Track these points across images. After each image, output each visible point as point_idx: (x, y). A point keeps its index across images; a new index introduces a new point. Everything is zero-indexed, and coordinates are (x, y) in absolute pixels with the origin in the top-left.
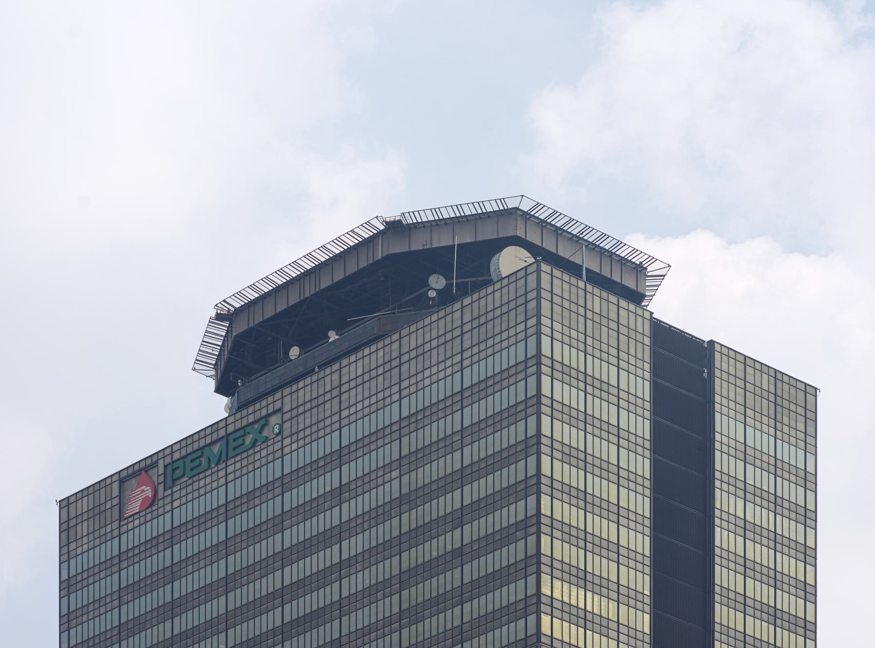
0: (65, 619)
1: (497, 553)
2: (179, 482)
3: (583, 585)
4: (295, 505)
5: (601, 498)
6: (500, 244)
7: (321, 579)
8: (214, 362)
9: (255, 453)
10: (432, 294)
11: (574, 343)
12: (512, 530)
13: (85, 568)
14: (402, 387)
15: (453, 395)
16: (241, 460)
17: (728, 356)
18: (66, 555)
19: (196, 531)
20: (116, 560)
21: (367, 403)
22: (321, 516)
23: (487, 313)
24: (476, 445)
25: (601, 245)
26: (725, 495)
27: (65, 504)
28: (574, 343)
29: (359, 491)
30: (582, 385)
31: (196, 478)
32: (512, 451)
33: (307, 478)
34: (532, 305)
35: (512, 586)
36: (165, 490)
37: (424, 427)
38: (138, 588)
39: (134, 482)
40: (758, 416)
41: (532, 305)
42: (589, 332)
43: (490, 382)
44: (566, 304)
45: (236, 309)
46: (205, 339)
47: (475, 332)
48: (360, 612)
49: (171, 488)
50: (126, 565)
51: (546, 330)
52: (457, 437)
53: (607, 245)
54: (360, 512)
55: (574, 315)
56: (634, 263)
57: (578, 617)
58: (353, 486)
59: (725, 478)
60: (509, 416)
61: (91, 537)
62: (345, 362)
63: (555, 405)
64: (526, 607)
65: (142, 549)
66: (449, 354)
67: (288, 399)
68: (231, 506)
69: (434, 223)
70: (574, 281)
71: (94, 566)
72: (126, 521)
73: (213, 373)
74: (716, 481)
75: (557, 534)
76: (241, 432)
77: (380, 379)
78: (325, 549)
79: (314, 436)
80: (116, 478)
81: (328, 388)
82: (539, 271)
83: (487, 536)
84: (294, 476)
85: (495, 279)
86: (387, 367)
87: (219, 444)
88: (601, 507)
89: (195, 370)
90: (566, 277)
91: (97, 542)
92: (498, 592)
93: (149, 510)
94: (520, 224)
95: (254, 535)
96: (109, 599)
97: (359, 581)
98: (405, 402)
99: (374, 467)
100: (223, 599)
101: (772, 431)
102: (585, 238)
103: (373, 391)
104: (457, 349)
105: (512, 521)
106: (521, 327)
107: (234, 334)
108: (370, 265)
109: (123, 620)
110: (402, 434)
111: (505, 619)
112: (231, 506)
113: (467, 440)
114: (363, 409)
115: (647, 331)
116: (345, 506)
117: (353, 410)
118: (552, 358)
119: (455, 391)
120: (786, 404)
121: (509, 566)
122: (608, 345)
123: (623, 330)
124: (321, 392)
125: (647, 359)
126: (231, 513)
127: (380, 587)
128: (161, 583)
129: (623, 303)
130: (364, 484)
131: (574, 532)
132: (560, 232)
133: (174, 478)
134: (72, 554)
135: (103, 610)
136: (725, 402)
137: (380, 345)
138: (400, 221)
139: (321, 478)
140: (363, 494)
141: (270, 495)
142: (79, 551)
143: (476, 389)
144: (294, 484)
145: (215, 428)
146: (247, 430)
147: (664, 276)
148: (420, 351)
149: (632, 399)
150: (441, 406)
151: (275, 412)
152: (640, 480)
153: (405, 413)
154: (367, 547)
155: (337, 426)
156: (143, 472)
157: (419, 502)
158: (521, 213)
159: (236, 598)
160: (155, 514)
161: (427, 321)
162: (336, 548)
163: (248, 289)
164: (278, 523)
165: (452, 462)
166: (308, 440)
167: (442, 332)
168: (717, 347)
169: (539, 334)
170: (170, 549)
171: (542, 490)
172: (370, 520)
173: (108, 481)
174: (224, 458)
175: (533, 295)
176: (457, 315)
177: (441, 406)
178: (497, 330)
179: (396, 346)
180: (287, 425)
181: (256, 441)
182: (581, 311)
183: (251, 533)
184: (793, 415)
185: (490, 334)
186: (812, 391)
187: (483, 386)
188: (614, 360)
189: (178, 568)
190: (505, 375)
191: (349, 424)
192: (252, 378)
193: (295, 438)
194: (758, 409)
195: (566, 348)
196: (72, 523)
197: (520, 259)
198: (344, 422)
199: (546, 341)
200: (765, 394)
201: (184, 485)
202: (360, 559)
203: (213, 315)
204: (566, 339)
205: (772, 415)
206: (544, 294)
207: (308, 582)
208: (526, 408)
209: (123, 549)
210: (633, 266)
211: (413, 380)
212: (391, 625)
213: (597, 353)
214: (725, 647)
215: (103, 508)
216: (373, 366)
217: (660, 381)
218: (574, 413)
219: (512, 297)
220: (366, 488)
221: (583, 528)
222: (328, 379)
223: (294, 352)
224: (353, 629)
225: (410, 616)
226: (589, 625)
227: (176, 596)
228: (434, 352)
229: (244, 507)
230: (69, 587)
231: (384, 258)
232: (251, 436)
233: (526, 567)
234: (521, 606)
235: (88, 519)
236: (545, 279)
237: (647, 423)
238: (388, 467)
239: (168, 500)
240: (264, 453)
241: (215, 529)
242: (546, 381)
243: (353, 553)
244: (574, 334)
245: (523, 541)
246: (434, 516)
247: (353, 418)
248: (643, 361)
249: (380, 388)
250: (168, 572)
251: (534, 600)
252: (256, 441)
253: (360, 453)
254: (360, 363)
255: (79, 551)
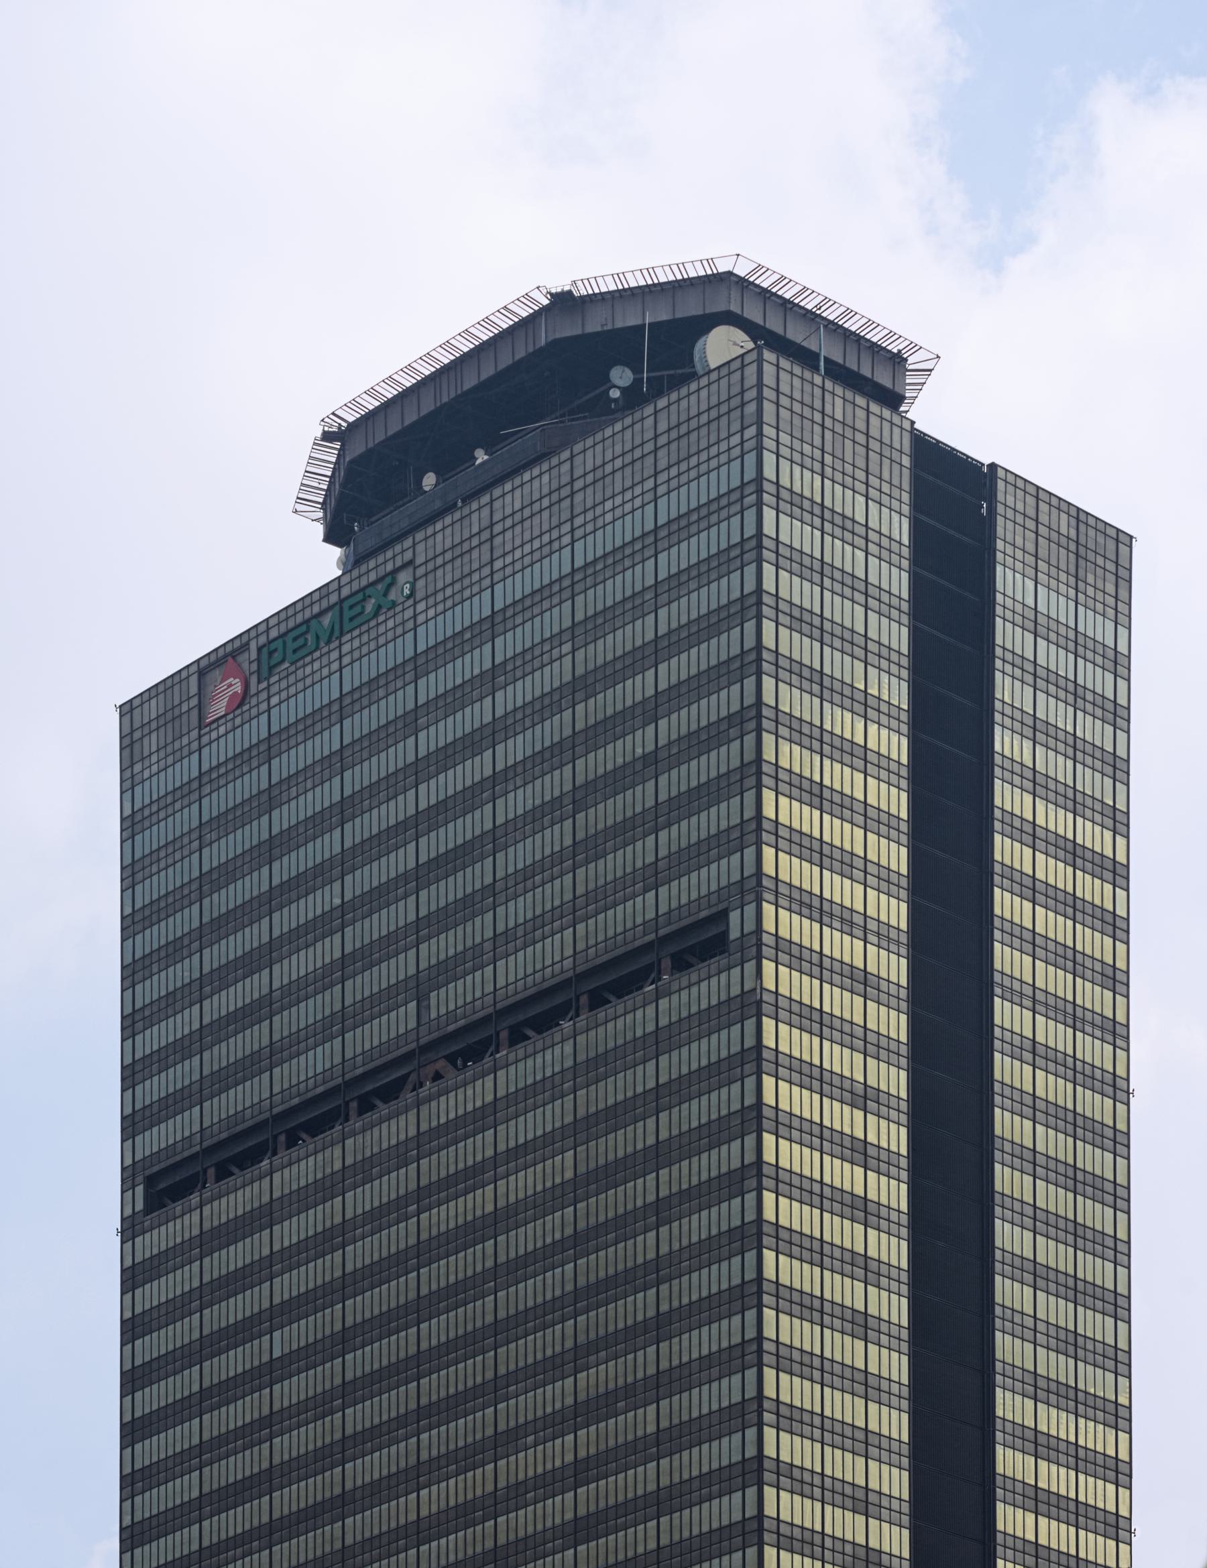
0: (128, 872)
1: (704, 758)
2: (278, 670)
3: (818, 805)
4: (432, 695)
5: (842, 682)
6: (706, 323)
7: (468, 800)
8: (321, 500)
9: (378, 625)
10: (615, 394)
11: (808, 462)
12: (724, 726)
13: (155, 797)
14: (576, 525)
15: (644, 535)
16: (360, 635)
17: (1015, 486)
18: (129, 782)
19: (300, 738)
20: (195, 785)
21: (527, 548)
22: (468, 710)
23: (689, 420)
24: (674, 605)
25: (846, 325)
26: (1008, 680)
27: (127, 710)
28: (808, 462)
29: (519, 673)
30: (817, 522)
31: (300, 663)
32: (723, 614)
33: (448, 657)
34: (751, 408)
35: (724, 805)
36: (259, 682)
37: (604, 581)
38: (224, 823)
39: (217, 674)
40: (1053, 571)
41: (751, 408)
42: (828, 448)
43: (694, 517)
44: (797, 407)
45: (349, 424)
46: (309, 469)
47: (674, 446)
48: (520, 846)
49: (268, 679)
50: (208, 791)
51: (769, 444)
52: (649, 595)
53: (853, 325)
54: (519, 703)
55: (807, 423)
56: (890, 351)
57: (811, 850)
58: (509, 667)
59: (1009, 656)
60: (719, 565)
61: (162, 754)
62: (497, 492)
63: (782, 550)
64: (742, 835)
65: (230, 766)
66: (638, 478)
67: (421, 546)
68: (347, 701)
69: (617, 295)
70: (807, 375)
71: (167, 794)
72: (207, 729)
73: (321, 515)
74: (996, 768)
75: (783, 731)
76: (360, 596)
77: (546, 514)
78: (474, 756)
79: (458, 598)
80: (194, 668)
81: (475, 530)
82: (760, 361)
83: (689, 734)
84: (431, 655)
85: (701, 372)
86: (555, 497)
87: (330, 614)
88: (842, 694)
89: (296, 512)
90: (797, 370)
91: (170, 760)
92: (704, 815)
93: (238, 712)
94: (735, 294)
95: (376, 741)
96: (186, 840)
97: (519, 801)
98: (579, 546)
99: (537, 640)
100: (337, 833)
101: (1072, 592)
102: (824, 315)
103: (536, 532)
104: (649, 471)
105: (724, 713)
106: (736, 440)
107: (347, 459)
108: (530, 354)
109: (205, 869)
110: (576, 591)
111: (714, 852)
112: (347, 701)
113: (664, 598)
114: (522, 557)
115: (907, 447)
116: (499, 695)
117: (509, 559)
118: (777, 484)
119: (647, 584)
120: (1091, 556)
121: (719, 777)
122: (854, 466)
123: (874, 445)
124: (466, 535)
125: (906, 486)
126: (347, 710)
127: (547, 809)
128: (255, 814)
129: (875, 408)
130: (526, 663)
131: (806, 729)
132: (790, 306)
133: (272, 663)
134: (138, 779)
135: (178, 856)
136: (1009, 550)
137: (545, 466)
138: (570, 292)
139: (468, 657)
140: (523, 677)
141: (399, 683)
142: (146, 774)
143: (674, 527)
144: (431, 666)
145: (324, 592)
146: (368, 592)
147: (931, 370)
148: (599, 474)
149: (885, 542)
150: (628, 551)
151: (404, 566)
152: (894, 657)
153: (579, 563)
154: (529, 753)
155: (487, 582)
156: (230, 659)
157: (599, 687)
158: (735, 279)
159: (358, 830)
160: (246, 716)
161: (608, 432)
162: (488, 754)
163: (365, 396)
164: (410, 723)
165: (643, 630)
166: (449, 603)
167: (628, 447)
168: (1001, 473)
169: (760, 449)
170: (267, 765)
171: (764, 613)
172: (534, 713)
173: (184, 675)
174: (337, 633)
175: (752, 394)
176: (649, 422)
177: (628, 551)
178: (703, 444)
179: (566, 467)
180: (421, 584)
181: (380, 607)
182: (818, 417)
183: (374, 738)
184: (1100, 571)
185: (693, 450)
186: (1127, 540)
187: (683, 523)
188: (861, 487)
189: (277, 792)
190: (714, 507)
191: (504, 579)
192: (373, 519)
193: (431, 601)
194: (1054, 562)
195: (797, 469)
196: (137, 735)
197: (735, 344)
198: (497, 577)
199: (769, 459)
200: (1063, 541)
201: (284, 674)
202: (520, 769)
203: (319, 434)
204: (797, 457)
205: (1072, 570)
206: (767, 393)
207: (450, 804)
208: (742, 553)
209: (205, 767)
210: (889, 355)
211: (590, 515)
212: (562, 863)
213: (838, 477)
214: (1010, 1566)
215: (177, 712)
216: (536, 496)
217: (923, 518)
218: (807, 561)
219: (724, 397)
220: (528, 668)
221: (818, 724)
222: (475, 516)
223: (429, 480)
224: (511, 870)
225: (587, 851)
226: (826, 861)
227: (275, 831)
228: (618, 475)
229: (365, 701)
230: (133, 824)
231: (548, 344)
232: (373, 601)
233: (742, 779)
234: (735, 834)
235: (157, 729)
236: (769, 371)
237: (905, 576)
238: (556, 639)
239: (264, 695)
240: (390, 624)
241: (326, 734)
242: (769, 515)
243: (511, 762)
244: (807, 449)
245: (738, 741)
246: (619, 707)
247: (508, 571)
248: (901, 489)
249: (545, 527)
250: (264, 798)
251: (753, 826)
252: (380, 607)
253: (519, 620)
254: (518, 493)
255: (146, 774)
